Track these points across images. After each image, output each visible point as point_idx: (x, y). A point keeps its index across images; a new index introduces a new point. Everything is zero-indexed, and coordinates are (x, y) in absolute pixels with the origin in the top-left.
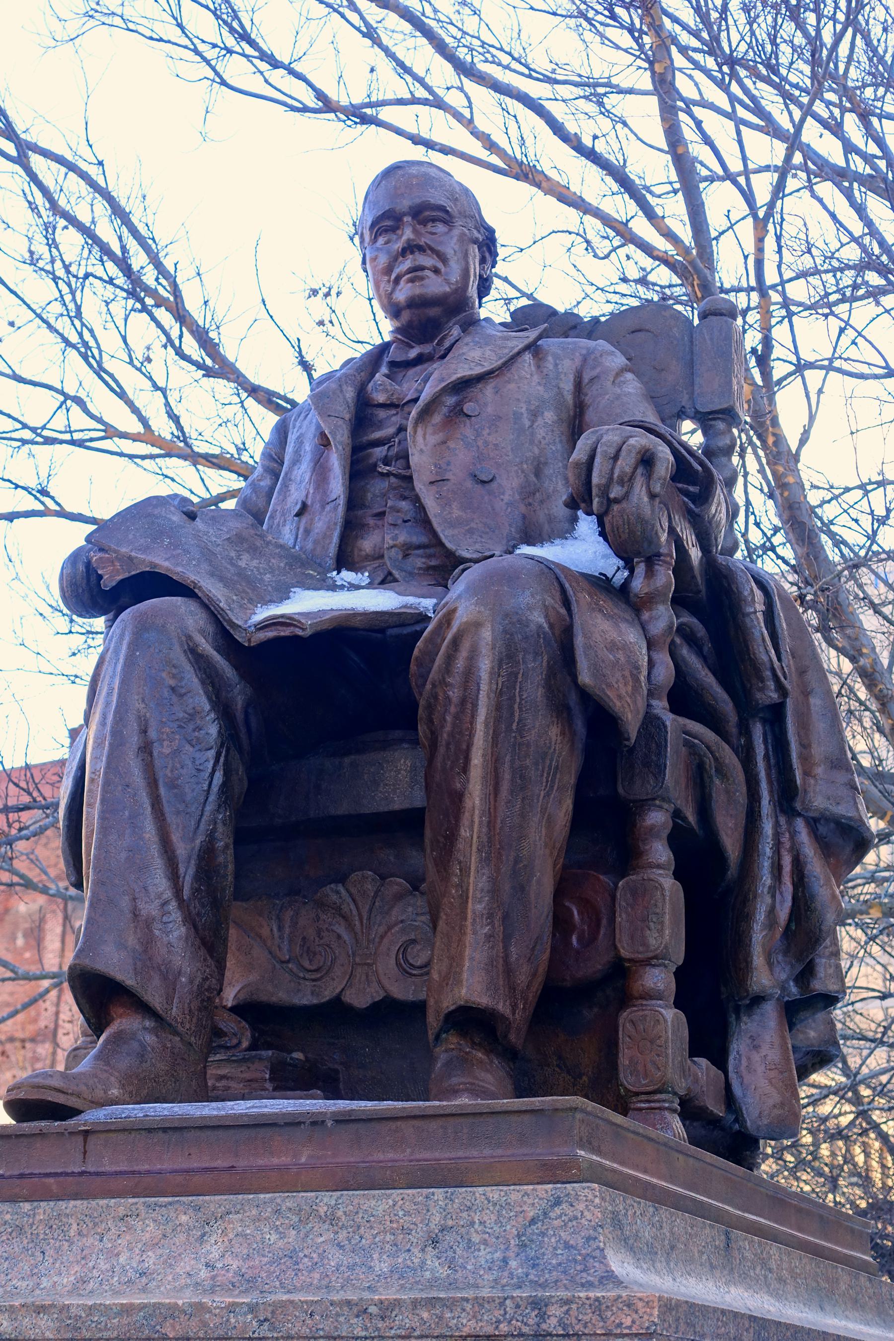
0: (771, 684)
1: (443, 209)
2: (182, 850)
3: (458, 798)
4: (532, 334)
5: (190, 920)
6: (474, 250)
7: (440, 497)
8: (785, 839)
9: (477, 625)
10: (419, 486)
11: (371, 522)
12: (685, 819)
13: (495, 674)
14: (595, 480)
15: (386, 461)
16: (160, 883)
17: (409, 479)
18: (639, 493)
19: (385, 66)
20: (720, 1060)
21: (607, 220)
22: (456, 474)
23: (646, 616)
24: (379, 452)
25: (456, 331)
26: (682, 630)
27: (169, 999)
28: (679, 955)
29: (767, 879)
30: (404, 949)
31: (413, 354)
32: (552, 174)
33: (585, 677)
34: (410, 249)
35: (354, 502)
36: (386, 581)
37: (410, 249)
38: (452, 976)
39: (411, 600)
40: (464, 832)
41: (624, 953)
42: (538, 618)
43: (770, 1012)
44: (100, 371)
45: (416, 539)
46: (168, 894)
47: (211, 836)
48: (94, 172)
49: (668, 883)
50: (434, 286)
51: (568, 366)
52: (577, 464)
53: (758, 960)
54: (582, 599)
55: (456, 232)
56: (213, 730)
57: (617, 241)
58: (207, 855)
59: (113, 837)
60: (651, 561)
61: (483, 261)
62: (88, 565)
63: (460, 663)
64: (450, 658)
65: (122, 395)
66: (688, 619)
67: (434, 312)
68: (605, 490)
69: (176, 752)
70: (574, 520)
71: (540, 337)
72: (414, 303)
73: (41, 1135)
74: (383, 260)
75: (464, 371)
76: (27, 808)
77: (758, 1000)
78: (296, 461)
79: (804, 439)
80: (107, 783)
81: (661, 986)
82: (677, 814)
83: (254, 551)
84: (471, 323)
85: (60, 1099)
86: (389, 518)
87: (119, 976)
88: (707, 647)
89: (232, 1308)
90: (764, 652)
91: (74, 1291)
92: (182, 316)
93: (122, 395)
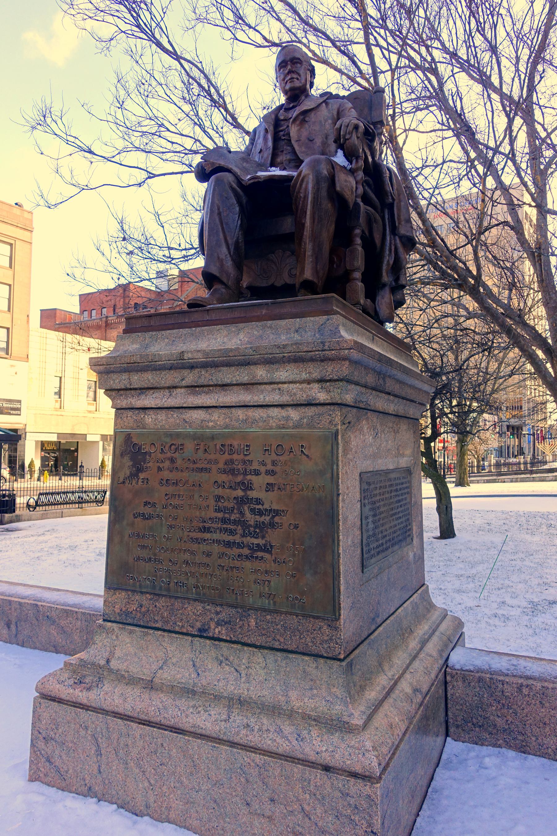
0: (390, 197)
1: (299, 59)
2: (230, 242)
3: (303, 225)
4: (325, 98)
5: (232, 260)
6: (308, 73)
7: (299, 145)
8: (393, 242)
9: (309, 174)
10: (293, 142)
11: (280, 153)
12: (365, 234)
13: (313, 188)
14: (342, 133)
15: (284, 136)
16: (224, 249)
17: (290, 140)
18: (354, 136)
19: (284, 30)
20: (374, 301)
21: (349, 77)
22: (303, 138)
23: (355, 174)
24: (282, 133)
25: (303, 98)
26: (365, 181)
27: (228, 280)
28: (363, 269)
29: (387, 252)
30: (290, 270)
31: (291, 105)
32: (333, 63)
33: (338, 189)
34: (290, 72)
35: (275, 148)
36: (284, 169)
37: (290, 72)
38: (302, 271)
39: (290, 173)
40: (305, 233)
41: (348, 268)
42: (325, 172)
43: (387, 289)
44: (205, 131)
45: (292, 158)
46: (227, 253)
47: (238, 238)
48: (199, 65)
49: (360, 249)
50: (297, 84)
51: (335, 107)
52: (337, 129)
53: (384, 274)
54: (337, 169)
55: (303, 67)
56: (237, 209)
57: (352, 83)
58: (237, 243)
59: (212, 237)
60: (357, 158)
61: (311, 77)
62: (202, 167)
63: (304, 186)
64: (301, 185)
65: (211, 138)
66: (367, 178)
67: (297, 92)
68: (344, 136)
69: (228, 215)
70: (336, 152)
71: (327, 99)
72: (292, 89)
73: (197, 311)
74: (282, 77)
75: (305, 108)
76: (191, 249)
77: (384, 285)
78: (259, 138)
79: (404, 143)
80: (209, 223)
81: (358, 277)
82: (363, 231)
83: (247, 162)
84: (307, 96)
85: (201, 303)
86: (285, 152)
87: (215, 274)
88: (373, 187)
89: (246, 348)
90: (389, 188)
91: (207, 347)
92: (226, 110)
93: (211, 138)
